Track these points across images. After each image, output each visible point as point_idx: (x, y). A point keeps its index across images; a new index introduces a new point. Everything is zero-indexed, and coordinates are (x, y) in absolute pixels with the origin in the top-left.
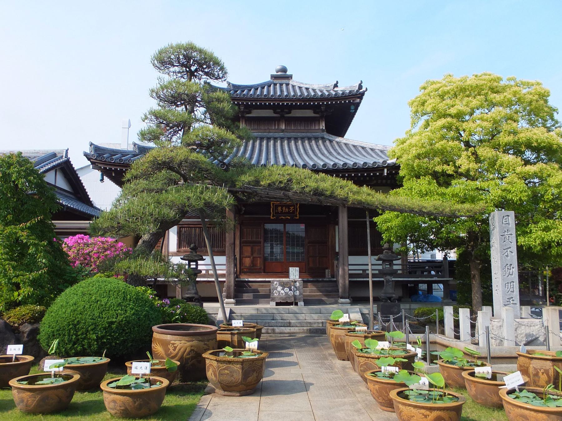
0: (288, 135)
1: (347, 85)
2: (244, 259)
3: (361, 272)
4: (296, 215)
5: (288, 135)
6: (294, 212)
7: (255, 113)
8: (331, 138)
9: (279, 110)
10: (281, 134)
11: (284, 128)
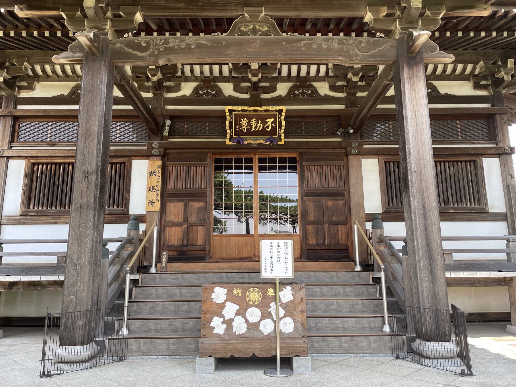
2: (168, 229)
4: (280, 136)
6: (274, 130)
9: (360, 94)
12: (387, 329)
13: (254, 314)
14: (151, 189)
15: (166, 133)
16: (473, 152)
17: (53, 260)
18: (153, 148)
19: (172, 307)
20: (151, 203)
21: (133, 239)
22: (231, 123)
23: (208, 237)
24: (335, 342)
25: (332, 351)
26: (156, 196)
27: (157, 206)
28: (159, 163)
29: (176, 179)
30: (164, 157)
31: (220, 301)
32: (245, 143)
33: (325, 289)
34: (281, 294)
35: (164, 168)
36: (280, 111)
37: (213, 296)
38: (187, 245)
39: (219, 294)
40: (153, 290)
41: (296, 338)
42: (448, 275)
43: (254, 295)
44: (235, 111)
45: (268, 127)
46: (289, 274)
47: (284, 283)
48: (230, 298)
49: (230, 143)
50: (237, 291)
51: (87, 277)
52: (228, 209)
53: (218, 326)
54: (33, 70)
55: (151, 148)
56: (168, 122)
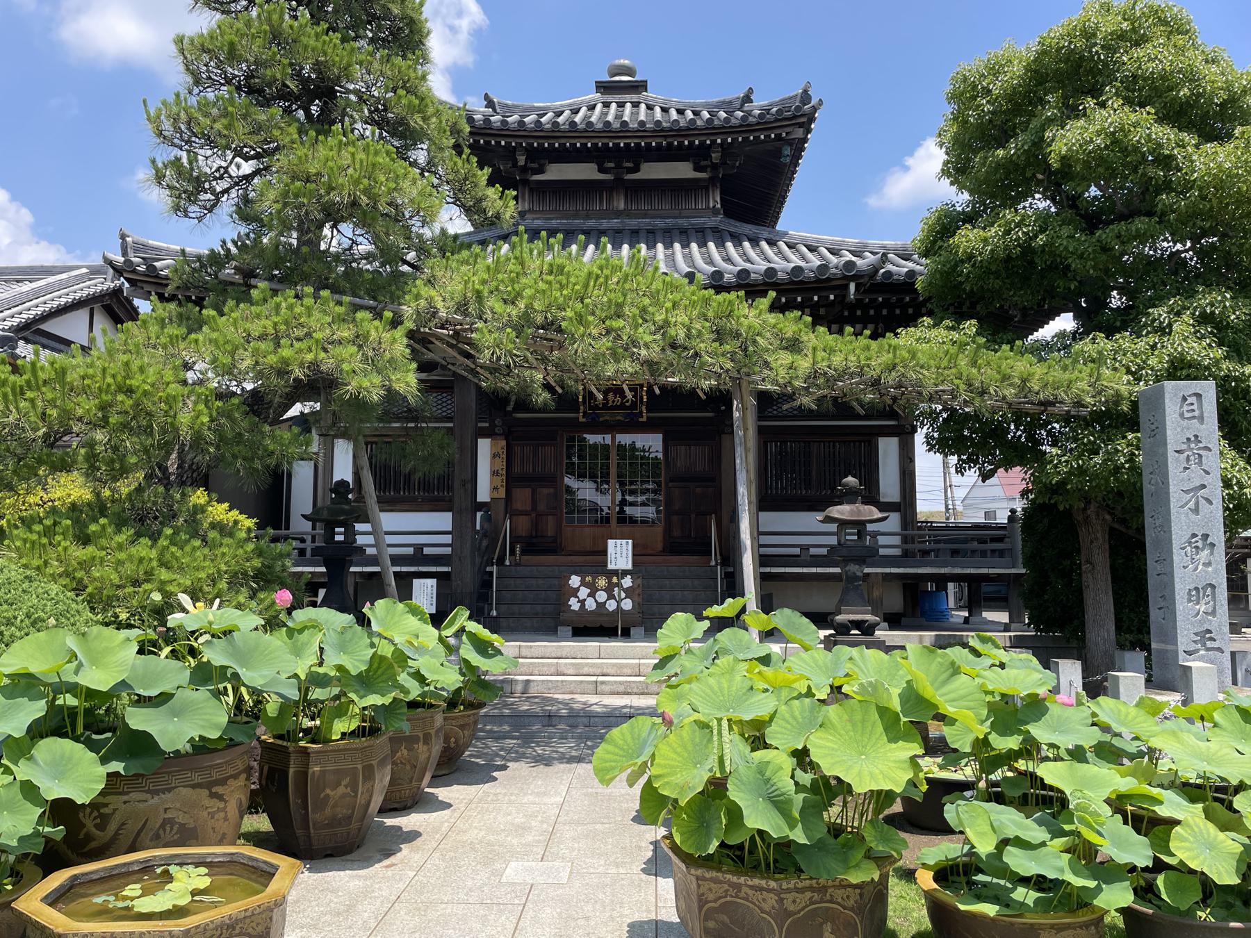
0: (633, 223)
1: (768, 96)
3: (797, 551)
4: (641, 412)
5: (633, 223)
6: (634, 405)
7: (556, 172)
8: (733, 230)
9: (612, 165)
10: (615, 223)
11: (622, 206)
13: (602, 596)
15: (510, 408)
17: (410, 551)
20: (495, 489)
23: (559, 527)
26: (500, 481)
27: (502, 493)
28: (504, 443)
31: (576, 586)
33: (674, 582)
35: (509, 447)
39: (575, 581)
40: (512, 581)
43: (602, 582)
46: (629, 566)
47: (625, 573)
48: (583, 584)
50: (589, 579)
53: (574, 604)
55: (493, 426)
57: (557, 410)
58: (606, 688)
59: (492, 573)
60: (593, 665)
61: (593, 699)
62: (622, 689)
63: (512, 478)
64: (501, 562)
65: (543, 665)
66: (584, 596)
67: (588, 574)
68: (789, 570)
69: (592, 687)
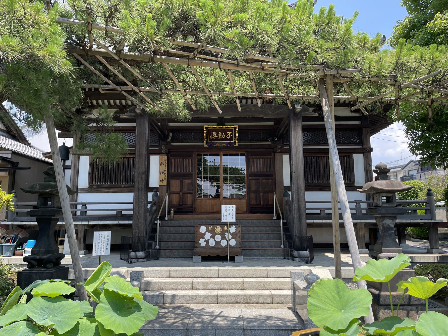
3: (318, 211)
6: (231, 138)
12: (282, 246)
13: (218, 238)
14: (161, 173)
15: (169, 140)
16: (348, 151)
17: (115, 213)
18: (162, 149)
19: (178, 236)
20: (162, 180)
21: (156, 202)
22: (207, 134)
23: (194, 200)
24: (257, 252)
25: (255, 256)
26: (164, 177)
27: (165, 183)
28: (166, 157)
29: (175, 166)
30: (168, 154)
31: (203, 232)
32: (215, 145)
33: (255, 228)
34: (230, 229)
35: (169, 160)
36: (235, 128)
37: (200, 230)
38: (182, 205)
39: (203, 229)
40: (168, 229)
41: (236, 248)
42: (308, 221)
43: (218, 229)
44: (209, 128)
45: (228, 136)
46: (234, 220)
47: (231, 224)
48: (208, 230)
49: (206, 146)
50: (211, 228)
51: (143, 221)
52: (205, 178)
53: (202, 242)
54: (92, 103)
55: (161, 149)
56: (171, 134)
57: (192, 121)
58: (224, 300)
59: (157, 224)
60: (215, 283)
61: (216, 309)
62: (233, 300)
63: (170, 175)
64: (162, 218)
65: (184, 283)
66: (208, 238)
67: (210, 225)
68: (315, 221)
69: (215, 299)
